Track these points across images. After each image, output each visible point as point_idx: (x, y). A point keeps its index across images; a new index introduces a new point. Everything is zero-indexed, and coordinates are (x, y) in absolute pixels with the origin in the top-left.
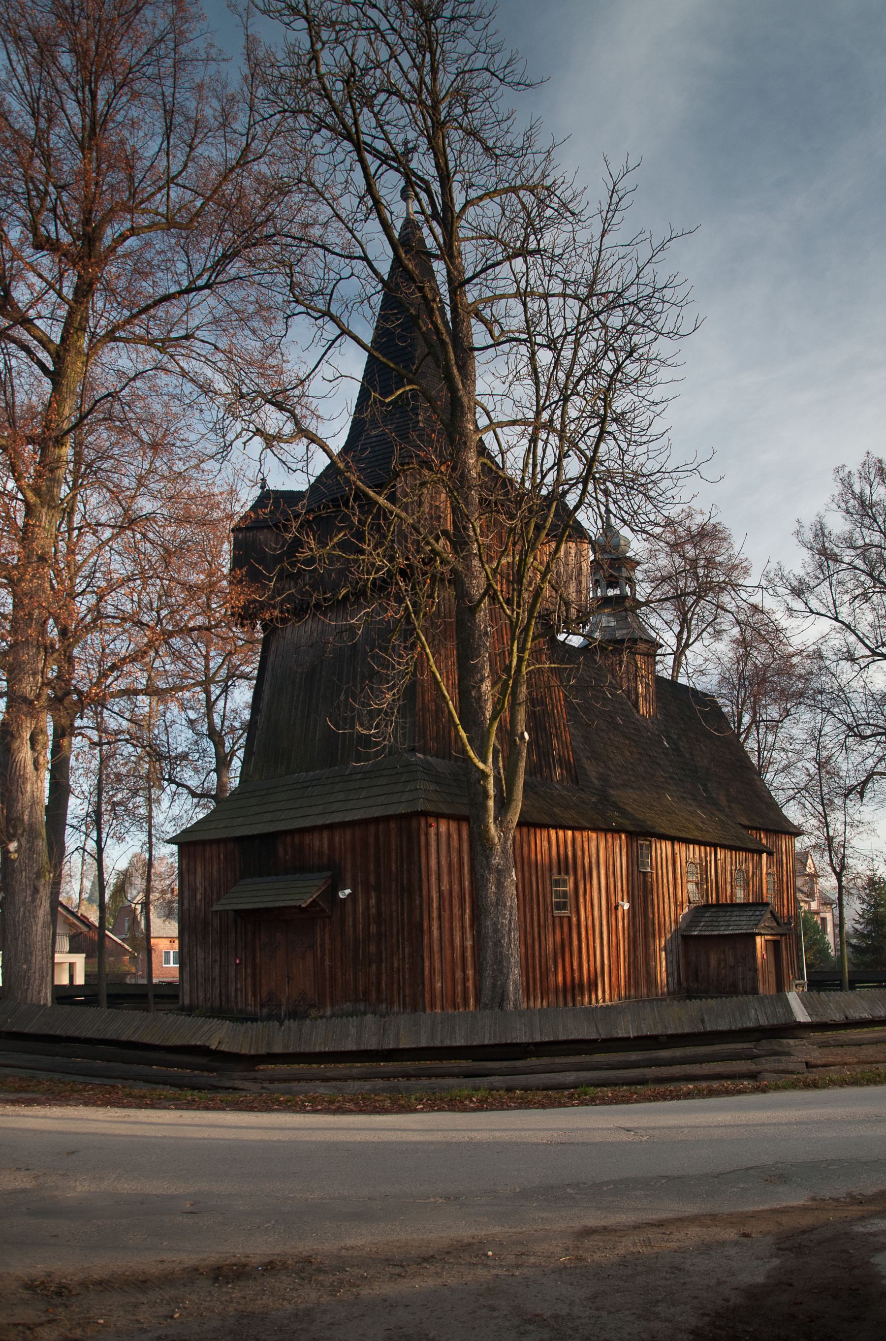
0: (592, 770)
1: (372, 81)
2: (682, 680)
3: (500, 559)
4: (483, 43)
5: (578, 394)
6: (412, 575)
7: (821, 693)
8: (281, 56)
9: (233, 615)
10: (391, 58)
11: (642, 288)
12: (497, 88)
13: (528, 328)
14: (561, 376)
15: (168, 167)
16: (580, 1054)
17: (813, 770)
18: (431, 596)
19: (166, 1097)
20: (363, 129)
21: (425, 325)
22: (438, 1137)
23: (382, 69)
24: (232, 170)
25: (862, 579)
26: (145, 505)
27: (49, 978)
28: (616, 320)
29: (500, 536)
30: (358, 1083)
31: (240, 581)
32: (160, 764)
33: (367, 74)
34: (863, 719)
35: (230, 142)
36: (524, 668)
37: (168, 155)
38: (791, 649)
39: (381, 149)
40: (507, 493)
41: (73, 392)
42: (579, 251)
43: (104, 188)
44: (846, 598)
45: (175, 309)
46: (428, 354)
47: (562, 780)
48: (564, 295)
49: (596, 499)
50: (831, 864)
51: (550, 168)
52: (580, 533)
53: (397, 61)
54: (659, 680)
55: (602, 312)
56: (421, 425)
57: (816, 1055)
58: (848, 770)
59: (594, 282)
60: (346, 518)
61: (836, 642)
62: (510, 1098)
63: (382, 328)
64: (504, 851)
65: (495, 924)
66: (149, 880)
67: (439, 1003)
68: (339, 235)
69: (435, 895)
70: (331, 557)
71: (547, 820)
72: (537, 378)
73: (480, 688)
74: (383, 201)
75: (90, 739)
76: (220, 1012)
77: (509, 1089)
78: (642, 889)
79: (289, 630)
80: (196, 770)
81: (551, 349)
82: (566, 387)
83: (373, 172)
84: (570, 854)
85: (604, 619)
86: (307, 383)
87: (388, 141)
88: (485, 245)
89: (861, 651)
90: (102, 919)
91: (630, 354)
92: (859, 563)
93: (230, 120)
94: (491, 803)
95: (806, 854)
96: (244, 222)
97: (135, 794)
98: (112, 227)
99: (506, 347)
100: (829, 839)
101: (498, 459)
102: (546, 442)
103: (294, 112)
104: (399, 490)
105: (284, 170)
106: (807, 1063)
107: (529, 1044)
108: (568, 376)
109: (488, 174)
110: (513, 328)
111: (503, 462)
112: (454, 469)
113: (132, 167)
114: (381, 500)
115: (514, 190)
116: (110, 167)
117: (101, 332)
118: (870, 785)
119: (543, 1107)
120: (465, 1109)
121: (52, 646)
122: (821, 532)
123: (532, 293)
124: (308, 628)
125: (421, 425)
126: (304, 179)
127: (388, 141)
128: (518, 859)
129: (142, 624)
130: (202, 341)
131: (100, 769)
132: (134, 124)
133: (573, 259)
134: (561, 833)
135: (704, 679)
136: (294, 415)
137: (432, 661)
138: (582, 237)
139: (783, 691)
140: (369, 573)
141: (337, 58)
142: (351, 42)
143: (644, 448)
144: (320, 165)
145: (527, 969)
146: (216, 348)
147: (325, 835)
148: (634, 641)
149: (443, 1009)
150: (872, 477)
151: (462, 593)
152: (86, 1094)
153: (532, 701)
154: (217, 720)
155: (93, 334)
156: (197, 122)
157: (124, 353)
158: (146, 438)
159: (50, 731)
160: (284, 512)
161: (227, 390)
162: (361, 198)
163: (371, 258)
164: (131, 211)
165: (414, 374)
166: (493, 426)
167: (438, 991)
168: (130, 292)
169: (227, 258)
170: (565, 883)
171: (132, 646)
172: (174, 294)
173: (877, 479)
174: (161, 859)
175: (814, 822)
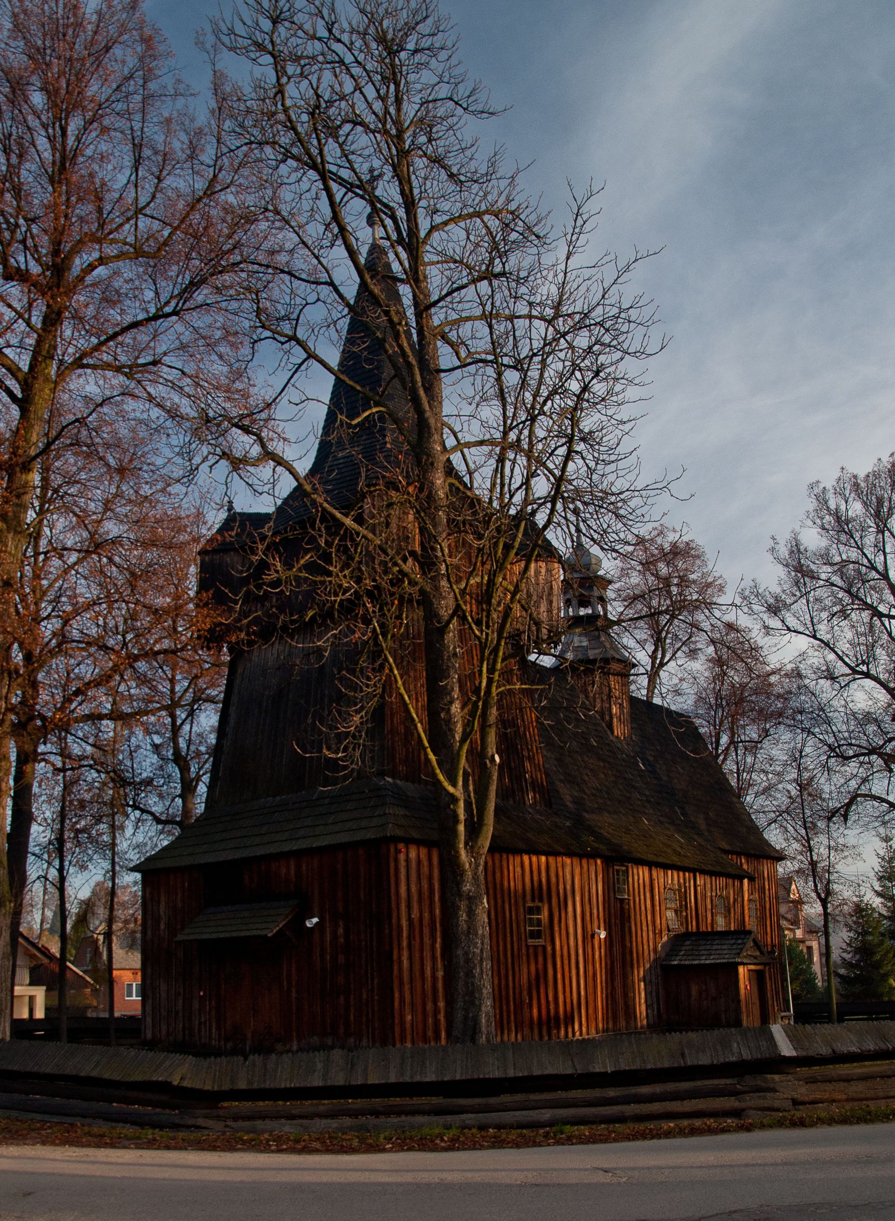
0: (567, 794)
1: (337, 112)
2: (657, 701)
5: (544, 414)
6: (380, 595)
7: (801, 713)
9: (199, 638)
10: (355, 90)
11: (608, 309)
12: (460, 118)
14: (528, 397)
15: (137, 199)
16: (556, 1090)
17: (794, 793)
18: (399, 617)
20: (329, 158)
21: (391, 348)
24: (199, 200)
25: (840, 596)
26: (112, 529)
27: (8, 1011)
28: (582, 341)
29: (468, 555)
32: (124, 789)
34: (845, 739)
35: (198, 173)
36: (494, 689)
37: (136, 187)
39: (346, 177)
40: (475, 513)
42: (545, 273)
43: (74, 220)
44: (824, 615)
47: (535, 803)
48: (530, 317)
49: (566, 518)
50: (816, 891)
52: (549, 552)
53: (362, 93)
54: (634, 701)
56: (388, 446)
57: (803, 1092)
60: (313, 540)
61: (815, 660)
62: (483, 1137)
64: (475, 877)
65: (466, 954)
66: (112, 909)
67: (409, 1037)
69: (404, 923)
70: (297, 579)
73: (449, 709)
75: (53, 765)
77: (482, 1128)
78: (619, 916)
79: (256, 653)
80: (161, 796)
81: (518, 370)
82: (533, 407)
84: (544, 880)
85: (576, 639)
87: (353, 170)
88: (450, 269)
90: (63, 950)
91: (597, 374)
92: (836, 579)
94: (461, 828)
95: (790, 880)
96: (211, 251)
97: (99, 821)
99: (472, 368)
101: (467, 479)
102: (514, 462)
104: (367, 511)
105: (250, 200)
108: (535, 396)
109: (453, 199)
111: (471, 482)
112: (421, 490)
113: (101, 200)
114: (348, 522)
116: (80, 199)
117: (69, 359)
118: (854, 807)
119: (517, 1146)
120: (435, 1149)
121: (17, 671)
122: (796, 549)
124: (275, 651)
127: (353, 170)
129: (107, 648)
131: (63, 796)
133: (539, 281)
134: (534, 859)
135: (680, 699)
136: (260, 440)
137: (400, 682)
139: (761, 710)
140: (336, 595)
142: (316, 76)
143: (612, 467)
144: (286, 194)
145: (500, 998)
146: (183, 373)
148: (606, 661)
149: (413, 1042)
151: (431, 614)
152: (43, 1132)
153: (503, 722)
154: (182, 744)
155: (61, 362)
156: (165, 155)
157: (91, 380)
158: (112, 462)
159: (13, 757)
160: (250, 535)
161: (193, 414)
162: (327, 226)
163: (337, 283)
164: (99, 241)
165: (381, 396)
166: (460, 446)
167: (408, 1026)
169: (194, 285)
170: (538, 910)
171: (97, 670)
172: (142, 321)
173: (853, 495)
174: (125, 887)
175: (796, 846)
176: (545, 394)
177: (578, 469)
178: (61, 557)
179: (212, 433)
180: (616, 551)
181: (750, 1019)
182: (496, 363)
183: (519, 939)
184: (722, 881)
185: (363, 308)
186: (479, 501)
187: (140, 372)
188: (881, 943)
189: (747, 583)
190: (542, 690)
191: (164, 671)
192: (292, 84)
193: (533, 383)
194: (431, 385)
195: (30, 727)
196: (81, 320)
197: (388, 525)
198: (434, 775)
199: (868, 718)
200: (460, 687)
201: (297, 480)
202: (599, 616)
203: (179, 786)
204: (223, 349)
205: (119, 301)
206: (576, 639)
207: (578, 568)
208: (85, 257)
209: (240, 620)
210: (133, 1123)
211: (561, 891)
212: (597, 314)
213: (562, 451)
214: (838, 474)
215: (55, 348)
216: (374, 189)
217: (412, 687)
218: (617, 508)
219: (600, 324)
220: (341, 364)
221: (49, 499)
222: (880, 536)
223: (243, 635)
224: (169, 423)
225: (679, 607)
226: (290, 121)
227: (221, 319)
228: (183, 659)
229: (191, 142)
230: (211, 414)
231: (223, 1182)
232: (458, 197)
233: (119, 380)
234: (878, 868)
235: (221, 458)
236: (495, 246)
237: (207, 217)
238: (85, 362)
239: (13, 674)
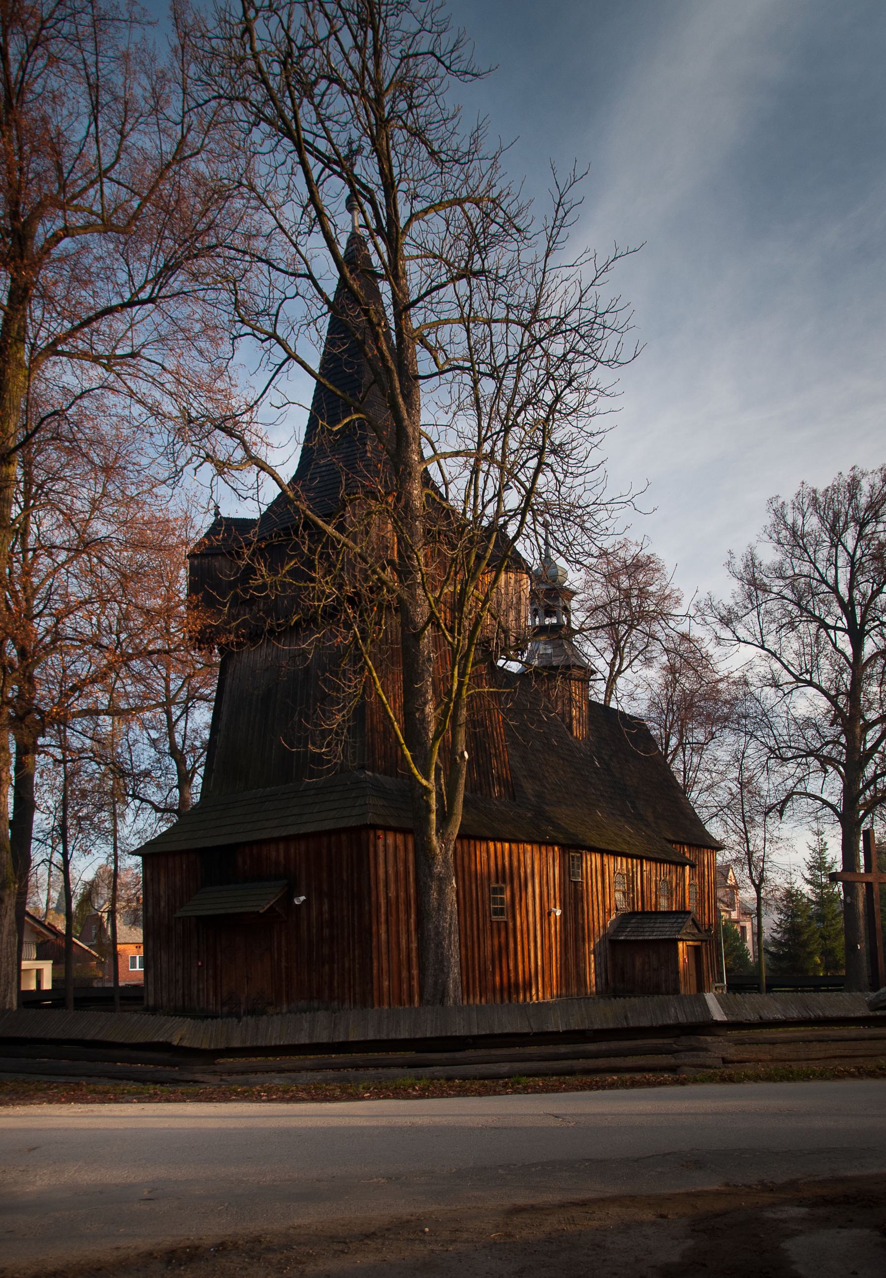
0: (529, 787)
1: (311, 64)
2: (613, 705)
3: (442, 589)
4: (428, 19)
5: (518, 425)
6: (360, 602)
7: (745, 717)
8: (211, 24)
9: (190, 639)
10: (330, 35)
11: (584, 313)
12: (443, 78)
13: (471, 355)
14: (503, 405)
15: (99, 157)
16: (514, 1046)
17: (735, 790)
18: (378, 623)
19: (129, 1092)
20: (304, 125)
21: (371, 351)
22: (383, 1122)
23: (322, 49)
24: (168, 166)
25: (790, 608)
26: (100, 528)
27: (15, 984)
28: (557, 347)
29: (443, 565)
30: (310, 1074)
31: (196, 607)
32: (123, 782)
33: (306, 55)
34: (785, 742)
35: (164, 131)
36: (464, 692)
37: (97, 142)
38: (717, 677)
39: (323, 150)
40: (450, 524)
41: (17, 408)
42: (524, 272)
43: (31, 176)
44: (773, 626)
45: (118, 324)
46: (374, 382)
47: (500, 796)
48: (507, 321)
49: (534, 530)
50: (751, 877)
51: (497, 176)
52: (518, 564)
53: (337, 39)
54: (592, 705)
55: (544, 338)
56: (369, 455)
57: (732, 1052)
58: (769, 790)
59: (537, 307)
60: (296, 547)
61: (762, 669)
62: (450, 1087)
63: (329, 353)
64: (445, 861)
65: (437, 927)
66: (115, 889)
67: (386, 1000)
68: (284, 249)
69: (383, 901)
70: (283, 584)
71: (487, 834)
72: (479, 409)
73: (423, 710)
74: (327, 213)
75: (53, 756)
76: (183, 1011)
77: (449, 1079)
78: (573, 897)
79: (245, 655)
80: (159, 786)
81: (494, 378)
82: (507, 418)
83: (315, 178)
84: (507, 864)
85: (541, 647)
86: (255, 408)
87: (330, 140)
88: (429, 265)
89: (786, 677)
90: (69, 927)
91: (569, 384)
92: (787, 593)
93: (162, 103)
94: (433, 817)
95: (728, 867)
96: (185, 230)
97: (100, 809)
98: (44, 224)
99: (449, 376)
100: (749, 854)
101: (442, 490)
102: (487, 474)
103: (230, 99)
104: (348, 520)
105: (224, 170)
106: (723, 1059)
107: (467, 1037)
108: (510, 405)
109: (433, 183)
110: (457, 356)
111: (447, 493)
112: (398, 499)
113: (59, 154)
114: (330, 529)
115: (459, 202)
116: (34, 150)
117: (42, 344)
118: (789, 804)
119: (480, 1094)
120: (408, 1097)
121: (11, 665)
122: (752, 563)
123: (476, 318)
124: (263, 653)
125: (369, 455)
126: (245, 182)
127: (330, 140)
128: (459, 869)
129: (101, 646)
130: (149, 360)
131: (65, 785)
132: (56, 98)
133: (518, 282)
134: (499, 845)
135: (634, 704)
136: (243, 443)
137: (378, 684)
138: (527, 257)
139: (709, 715)
140: (319, 600)
141: (273, 32)
142: (286, 11)
143: (580, 480)
144: (261, 166)
145: (466, 967)
146: (164, 368)
147: (282, 847)
148: (568, 667)
149: (390, 1005)
150: (805, 507)
151: (407, 620)
152: (50, 1092)
153: (472, 723)
154: (178, 739)
155: (33, 347)
156: (126, 103)
157: (68, 369)
158: (97, 460)
159: (13, 749)
160: (236, 539)
161: (176, 413)
162: (305, 208)
163: (316, 276)
164: (63, 207)
165: (361, 403)
166: (438, 456)
167: (385, 990)
168: (69, 302)
169: (168, 270)
170: (502, 891)
171: (93, 668)
172: (116, 307)
173: (810, 510)
174: (126, 870)
175: (735, 837)
176: (519, 405)
177: (548, 482)
178: (50, 555)
179: (195, 434)
180: (580, 563)
181: (687, 988)
182: (473, 370)
183: (484, 916)
184: (666, 867)
185: (343, 307)
186: (454, 511)
187: (118, 364)
188: (809, 925)
189: (702, 596)
190: (508, 694)
191: (158, 671)
192: (260, 21)
193: (509, 393)
194: (410, 392)
195: (29, 722)
196: (51, 299)
197: (367, 533)
198: (410, 769)
199: (809, 722)
200: (434, 692)
201: (280, 486)
202: (562, 626)
203: (176, 778)
204: (203, 344)
205: (91, 282)
206: (541, 647)
207: (544, 579)
208: (48, 224)
209: (230, 623)
210: (135, 1080)
211: (522, 875)
212: (573, 319)
213: (533, 463)
214: (797, 488)
215: (25, 328)
216: (353, 165)
217: (390, 688)
218: (584, 521)
219: (575, 330)
220: (322, 367)
221: (34, 494)
222: (834, 550)
223: (232, 637)
224: (151, 421)
225: (640, 617)
226: (260, 70)
227: (199, 311)
228: (177, 659)
229: (153, 89)
230: (194, 414)
231: (219, 1129)
232: (438, 180)
233: (97, 372)
234: (809, 858)
235: (205, 461)
236: (474, 236)
237: (177, 187)
238: (59, 348)
239: (6, 667)
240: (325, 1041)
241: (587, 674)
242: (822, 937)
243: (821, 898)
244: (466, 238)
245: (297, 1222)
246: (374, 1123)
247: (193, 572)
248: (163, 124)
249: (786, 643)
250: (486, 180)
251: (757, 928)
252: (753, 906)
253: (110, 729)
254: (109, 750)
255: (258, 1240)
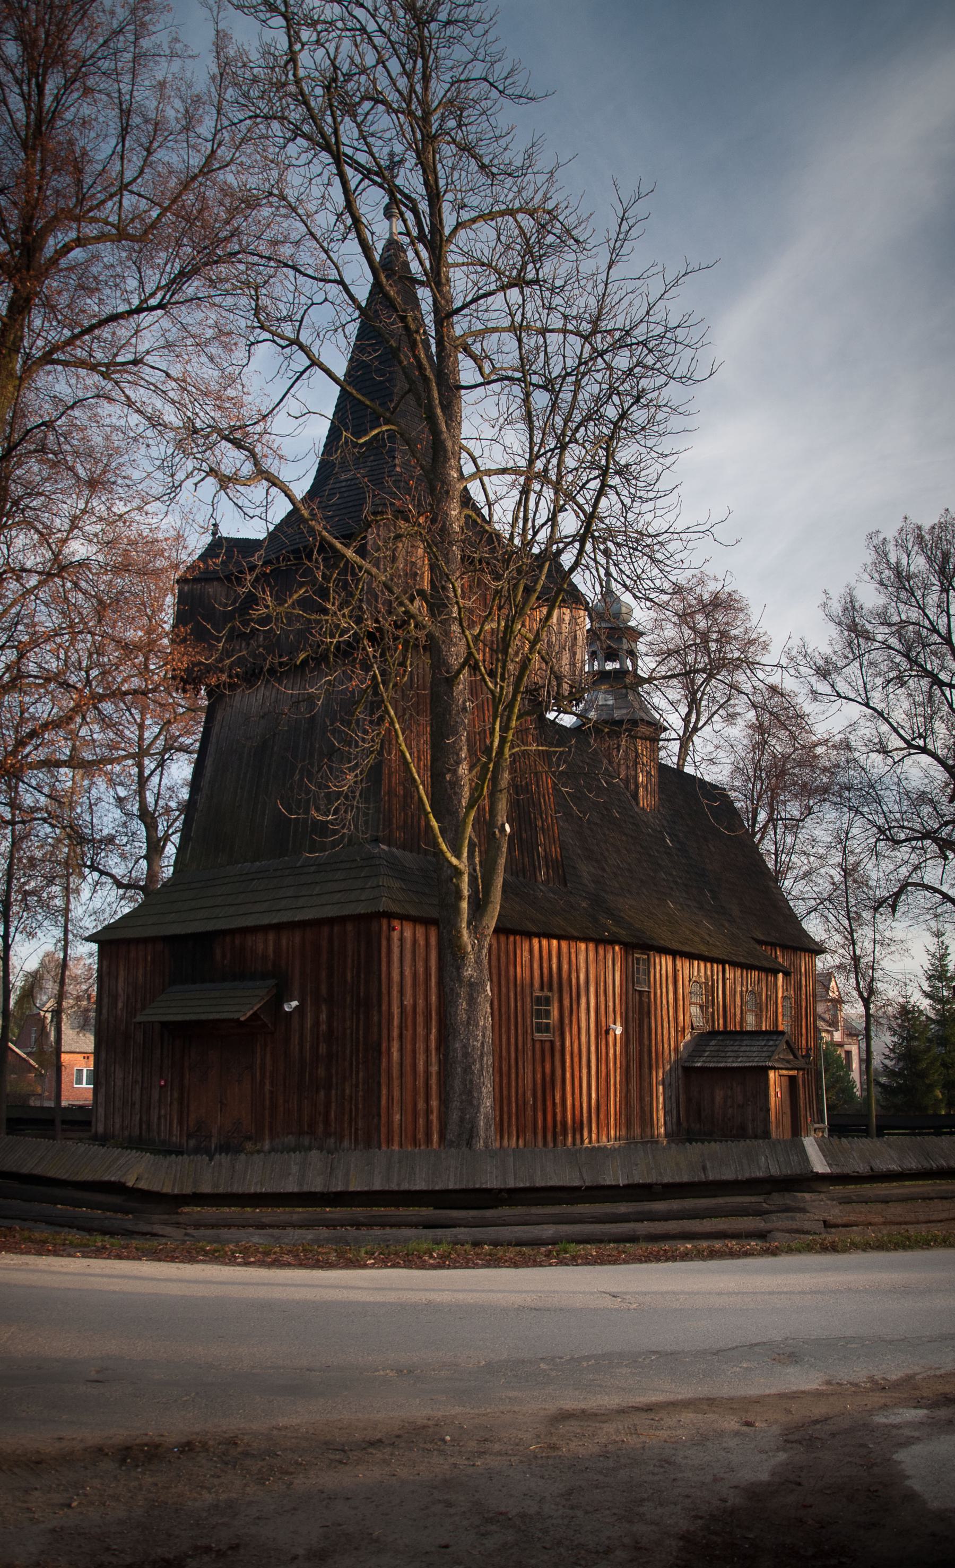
0: (586, 870)
2: (689, 770)
4: (482, 51)
5: (576, 442)
6: (382, 639)
7: (849, 789)
9: (174, 678)
10: (378, 64)
11: (652, 326)
12: (496, 101)
16: (560, 1203)
17: (838, 878)
18: (402, 664)
20: (344, 139)
21: (407, 359)
24: (194, 178)
25: (897, 660)
26: (78, 549)
28: (622, 361)
30: (298, 1232)
32: (81, 848)
34: (896, 820)
35: (194, 147)
36: (507, 750)
37: (122, 158)
39: (363, 162)
40: (493, 550)
42: (582, 283)
43: (48, 193)
44: (879, 681)
45: (123, 330)
46: (409, 391)
47: (548, 880)
48: (565, 331)
49: (595, 560)
50: (858, 988)
52: (575, 598)
53: (385, 67)
55: (606, 351)
56: (398, 469)
57: (836, 1213)
58: (878, 880)
59: (598, 318)
60: (308, 572)
61: (867, 731)
64: (478, 961)
65: (465, 1047)
66: (62, 983)
67: (396, 1139)
69: (396, 1011)
70: (289, 616)
74: (364, 220)
76: (139, 1143)
78: (639, 1011)
79: (238, 698)
80: (123, 856)
81: (548, 390)
83: (353, 187)
84: (554, 966)
85: (601, 696)
88: (476, 272)
89: (895, 742)
91: (637, 400)
92: (893, 642)
94: (464, 905)
95: (829, 976)
96: (205, 237)
97: (51, 881)
99: (496, 387)
100: (856, 959)
101: (485, 511)
102: (539, 494)
104: (370, 543)
105: (253, 181)
106: (825, 1222)
107: (501, 1190)
109: (483, 194)
111: (490, 515)
113: (81, 171)
114: (350, 553)
115: (511, 212)
118: (903, 897)
119: (516, 1265)
120: (423, 1266)
122: (851, 606)
123: (528, 327)
124: (260, 696)
125: (398, 469)
126: (276, 192)
128: (494, 971)
129: (69, 685)
131: (11, 852)
133: (576, 292)
135: (714, 768)
136: (253, 455)
137: (401, 738)
138: (587, 267)
139: (805, 785)
140: (333, 636)
142: (334, 44)
143: (650, 505)
144: (294, 178)
145: (501, 1100)
146: (168, 375)
148: (634, 723)
149: (401, 1145)
150: (910, 545)
151: (439, 662)
153: (516, 788)
154: (150, 798)
156: (157, 124)
160: (238, 563)
162: (339, 216)
163: (347, 282)
164: (78, 219)
165: (392, 413)
166: (480, 474)
169: (184, 276)
171: (55, 711)
172: (122, 313)
173: (916, 548)
175: (838, 938)
179: (198, 446)
183: (525, 1033)
184: (755, 974)
187: (119, 371)
188: (929, 1049)
190: (562, 753)
191: (131, 714)
196: (53, 308)
198: (436, 845)
199: (923, 798)
201: (293, 504)
203: (145, 846)
206: (601, 696)
212: (640, 333)
213: (595, 484)
219: (644, 344)
222: (944, 595)
226: (302, 93)
227: (213, 316)
234: (927, 966)
235: (208, 474)
240: (318, 1189)
241: (655, 730)
242: (944, 1065)
243: (943, 1015)
244: (519, 247)
245: (282, 1421)
246: (379, 1297)
247: (182, 599)
248: (192, 141)
249: (894, 702)
250: (541, 193)
251: (863, 1053)
252: (861, 1025)
253: (69, 784)
254: (67, 809)
255: (232, 1442)
